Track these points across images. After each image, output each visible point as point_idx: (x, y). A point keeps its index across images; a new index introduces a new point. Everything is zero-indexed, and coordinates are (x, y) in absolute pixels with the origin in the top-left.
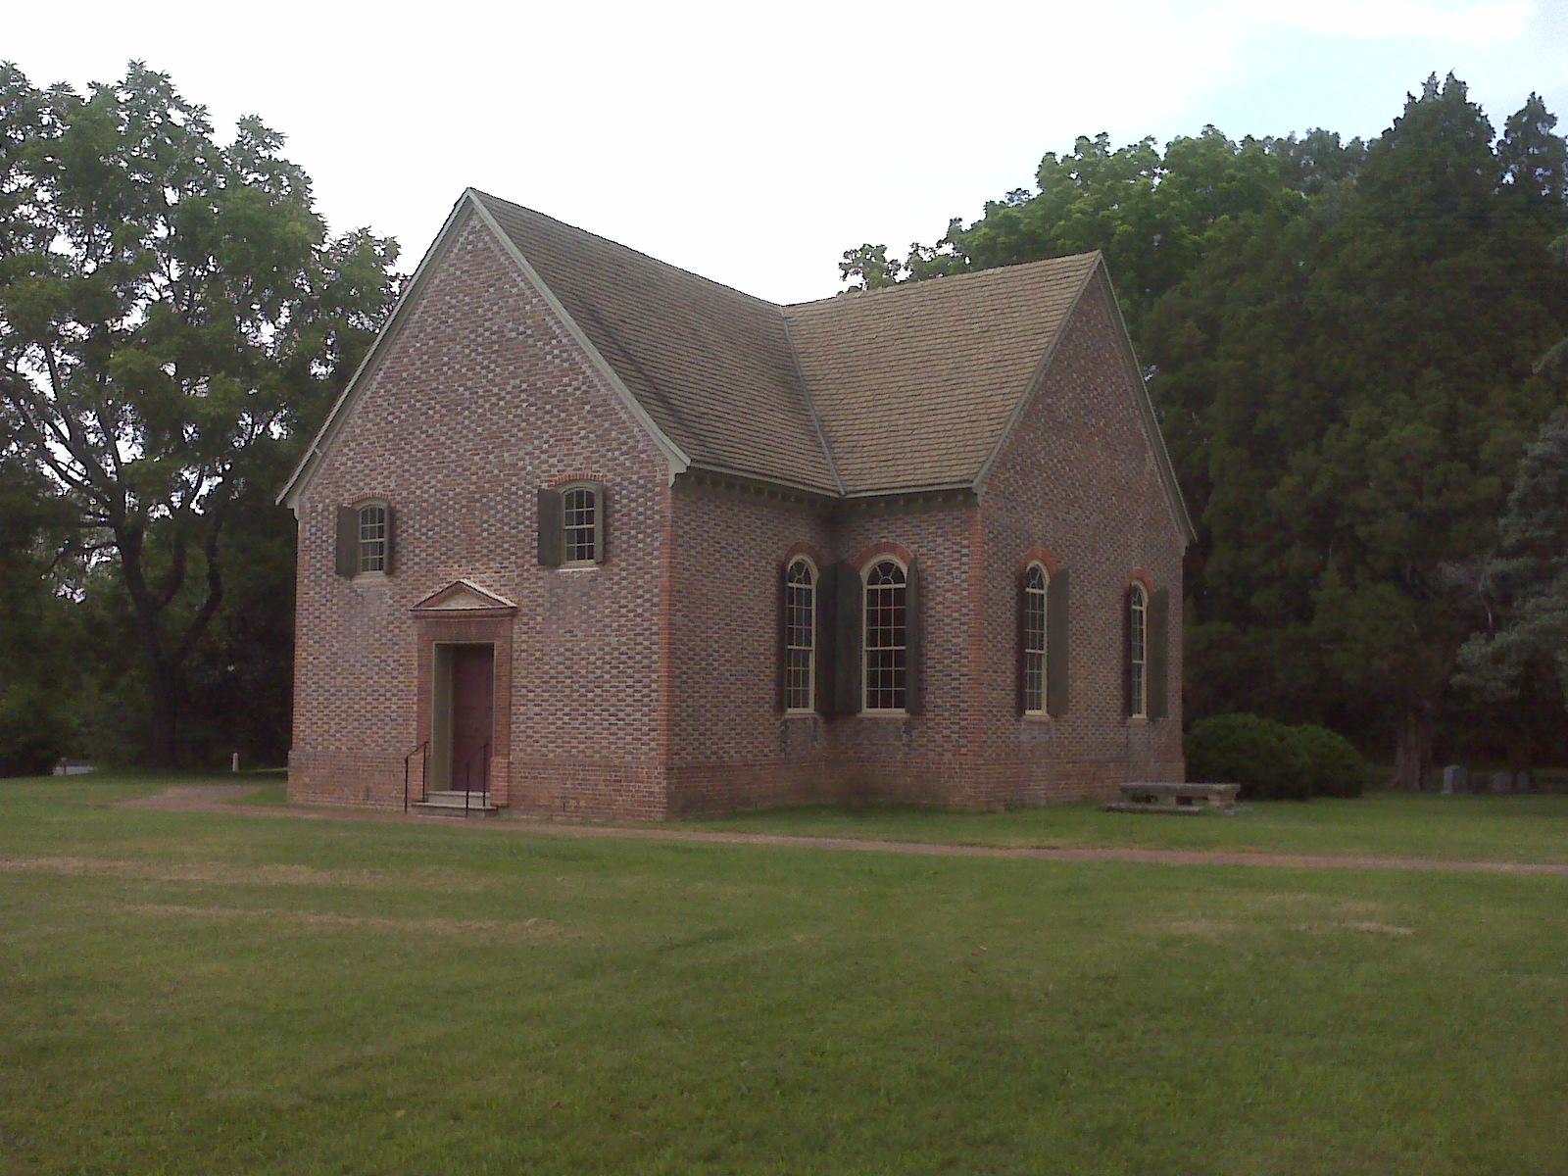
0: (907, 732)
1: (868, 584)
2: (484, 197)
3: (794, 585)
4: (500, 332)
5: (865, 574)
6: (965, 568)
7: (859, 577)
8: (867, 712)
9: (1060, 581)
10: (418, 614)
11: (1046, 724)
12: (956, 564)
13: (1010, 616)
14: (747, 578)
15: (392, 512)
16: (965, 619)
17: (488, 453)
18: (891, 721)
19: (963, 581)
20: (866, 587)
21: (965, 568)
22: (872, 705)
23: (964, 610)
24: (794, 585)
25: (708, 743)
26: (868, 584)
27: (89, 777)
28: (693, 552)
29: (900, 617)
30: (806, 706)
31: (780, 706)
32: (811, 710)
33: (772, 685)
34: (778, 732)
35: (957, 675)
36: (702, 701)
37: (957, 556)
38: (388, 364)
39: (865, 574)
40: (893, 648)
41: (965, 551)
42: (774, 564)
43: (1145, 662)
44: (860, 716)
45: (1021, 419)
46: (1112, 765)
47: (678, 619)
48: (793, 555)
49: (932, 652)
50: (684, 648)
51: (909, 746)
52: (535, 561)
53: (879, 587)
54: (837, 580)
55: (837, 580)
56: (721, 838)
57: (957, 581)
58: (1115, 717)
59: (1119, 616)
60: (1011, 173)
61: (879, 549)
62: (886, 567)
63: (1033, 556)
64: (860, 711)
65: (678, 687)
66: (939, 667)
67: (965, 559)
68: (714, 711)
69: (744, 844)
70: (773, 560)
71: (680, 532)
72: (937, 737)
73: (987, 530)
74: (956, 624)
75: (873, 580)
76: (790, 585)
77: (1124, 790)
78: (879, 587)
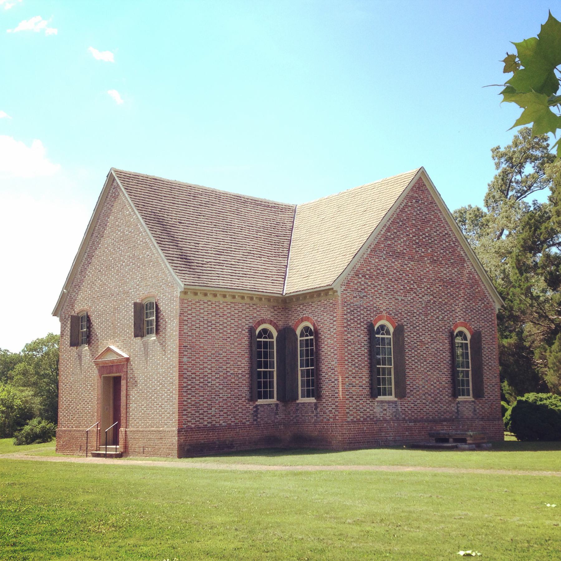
1: (300, 337)
3: (380, 336)
4: (123, 232)
5: (298, 332)
6: (335, 327)
7: (296, 334)
8: (301, 400)
9: (399, 330)
10: (97, 364)
12: (331, 325)
13: (365, 350)
14: (229, 338)
15: (88, 317)
16: (335, 352)
17: (119, 287)
18: (309, 404)
19: (334, 334)
20: (299, 339)
21: (335, 327)
23: (335, 348)
24: (380, 336)
26: (300, 337)
32: (274, 400)
34: (252, 412)
35: (333, 380)
37: (332, 321)
38: (88, 250)
39: (298, 332)
40: (263, 370)
41: (335, 319)
42: (247, 331)
43: (470, 369)
44: (298, 402)
45: (368, 253)
46: (445, 423)
47: (185, 359)
48: (259, 325)
49: (324, 368)
51: (316, 416)
52: (405, 327)
53: (262, 340)
54: (286, 334)
55: (286, 334)
57: (332, 334)
58: (446, 398)
59: (447, 346)
60: (515, 122)
61: (302, 320)
63: (380, 319)
64: (298, 399)
65: (185, 392)
66: (327, 376)
67: (335, 323)
69: (113, 465)
70: (247, 328)
71: (185, 318)
72: (327, 411)
73: (345, 308)
74: (332, 355)
75: (302, 335)
76: (312, 337)
77: (431, 435)
78: (262, 340)
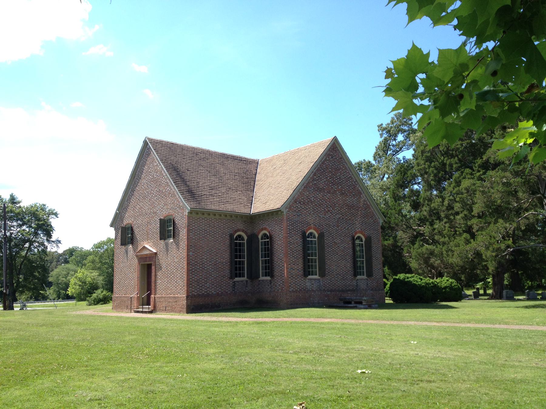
0: (270, 284)
2: (151, 140)
5: (260, 237)
8: (261, 278)
10: (137, 256)
11: (319, 280)
13: (300, 248)
20: (260, 241)
22: (262, 276)
25: (203, 289)
27: (488, 299)
28: (196, 234)
29: (236, 251)
30: (244, 276)
31: (355, 275)
32: (245, 278)
33: (228, 271)
36: (201, 277)
39: (260, 237)
46: (349, 292)
47: (191, 253)
50: (193, 262)
55: (252, 238)
56: (221, 319)
61: (262, 230)
62: (265, 235)
68: (205, 280)
71: (191, 228)
75: (262, 239)
